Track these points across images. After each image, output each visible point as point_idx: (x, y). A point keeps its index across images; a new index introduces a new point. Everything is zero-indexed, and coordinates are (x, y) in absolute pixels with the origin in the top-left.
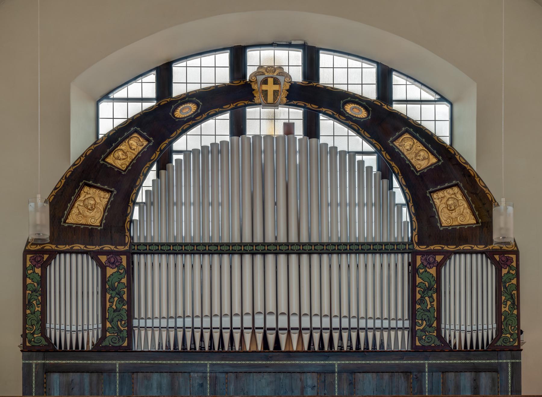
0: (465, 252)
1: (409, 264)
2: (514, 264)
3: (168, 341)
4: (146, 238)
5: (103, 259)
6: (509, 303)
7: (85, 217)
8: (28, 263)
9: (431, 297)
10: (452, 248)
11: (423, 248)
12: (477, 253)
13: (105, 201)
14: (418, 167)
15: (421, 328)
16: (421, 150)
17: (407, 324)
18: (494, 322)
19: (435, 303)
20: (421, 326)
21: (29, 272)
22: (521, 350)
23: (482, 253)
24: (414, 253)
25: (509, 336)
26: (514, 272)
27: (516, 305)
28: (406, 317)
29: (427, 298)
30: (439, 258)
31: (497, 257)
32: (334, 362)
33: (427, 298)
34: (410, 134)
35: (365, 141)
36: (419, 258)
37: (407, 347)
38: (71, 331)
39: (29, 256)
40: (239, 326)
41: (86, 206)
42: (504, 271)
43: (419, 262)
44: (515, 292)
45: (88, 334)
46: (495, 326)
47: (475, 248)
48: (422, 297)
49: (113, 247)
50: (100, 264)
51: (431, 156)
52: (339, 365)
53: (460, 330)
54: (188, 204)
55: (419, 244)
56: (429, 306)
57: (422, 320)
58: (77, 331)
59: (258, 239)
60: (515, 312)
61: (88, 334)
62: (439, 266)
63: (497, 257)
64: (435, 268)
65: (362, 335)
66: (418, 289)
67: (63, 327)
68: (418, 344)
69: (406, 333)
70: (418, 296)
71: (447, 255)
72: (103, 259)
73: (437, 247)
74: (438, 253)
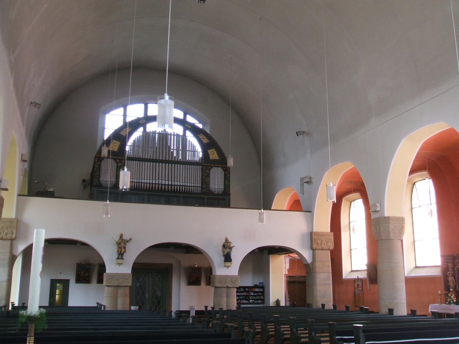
0: (216, 167)
1: (201, 169)
2: (229, 171)
3: (105, 184)
4: (129, 155)
5: (118, 161)
6: (227, 181)
7: (113, 148)
8: (96, 160)
9: (207, 178)
10: (213, 165)
11: (205, 165)
12: (219, 167)
13: (119, 144)
14: (204, 142)
15: (204, 187)
16: (205, 138)
17: (200, 185)
18: (223, 186)
19: (208, 180)
20: (205, 186)
21: (96, 163)
22: (230, 194)
23: (220, 167)
24: (203, 166)
25: (227, 190)
26: (228, 173)
27: (229, 182)
28: (200, 183)
29: (206, 179)
30: (209, 168)
31: (224, 169)
32: (181, 195)
33: (206, 179)
34: (202, 133)
35: (104, 128)
36: (204, 167)
37: (200, 192)
38: (216, 188)
39: (96, 158)
40: (158, 183)
41: (113, 145)
42: (226, 173)
43: (204, 168)
44: (229, 178)
45: (219, 189)
46: (223, 187)
47: (219, 166)
48: (205, 178)
49: (120, 158)
50: (116, 162)
51: (208, 140)
52: (182, 196)
53: (213, 188)
54: (189, 151)
55: (204, 163)
56: (207, 181)
57: (205, 184)
58: (219, 188)
59: (161, 159)
60: (229, 184)
61: (219, 189)
62: (210, 170)
63: (224, 169)
64: (208, 171)
65: (176, 187)
66: (204, 176)
67: (214, 187)
68: (203, 191)
69: (200, 188)
70: (204, 178)
71: (212, 167)
72: (118, 161)
73: (209, 165)
74: (210, 166)
